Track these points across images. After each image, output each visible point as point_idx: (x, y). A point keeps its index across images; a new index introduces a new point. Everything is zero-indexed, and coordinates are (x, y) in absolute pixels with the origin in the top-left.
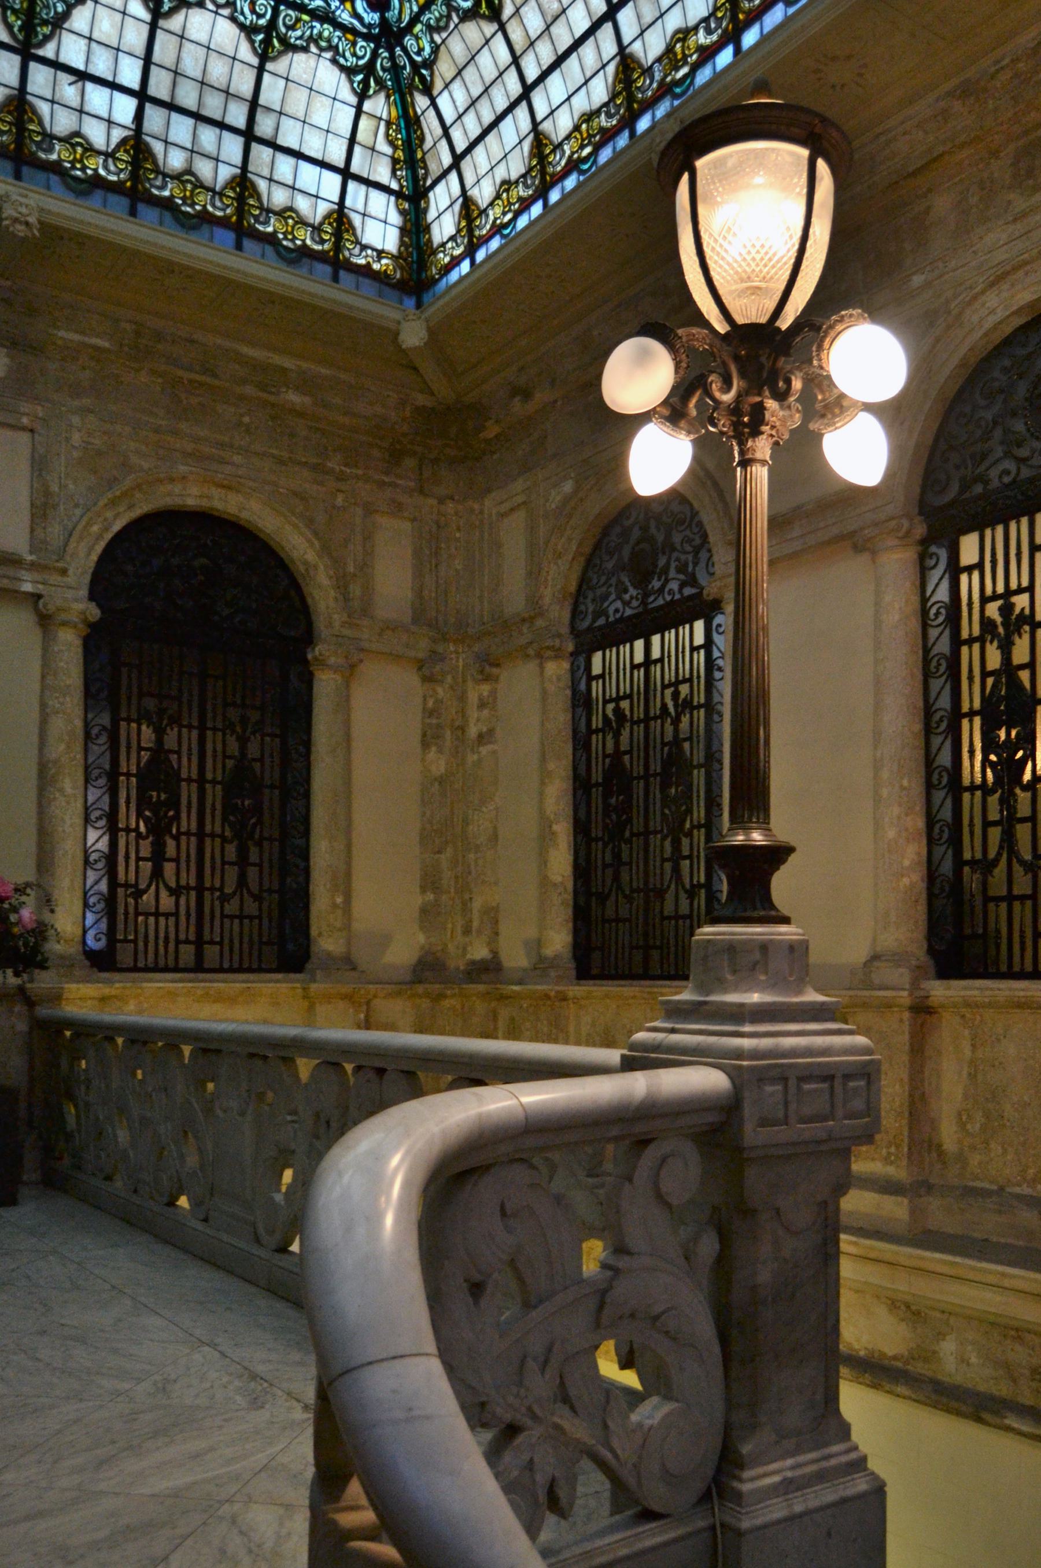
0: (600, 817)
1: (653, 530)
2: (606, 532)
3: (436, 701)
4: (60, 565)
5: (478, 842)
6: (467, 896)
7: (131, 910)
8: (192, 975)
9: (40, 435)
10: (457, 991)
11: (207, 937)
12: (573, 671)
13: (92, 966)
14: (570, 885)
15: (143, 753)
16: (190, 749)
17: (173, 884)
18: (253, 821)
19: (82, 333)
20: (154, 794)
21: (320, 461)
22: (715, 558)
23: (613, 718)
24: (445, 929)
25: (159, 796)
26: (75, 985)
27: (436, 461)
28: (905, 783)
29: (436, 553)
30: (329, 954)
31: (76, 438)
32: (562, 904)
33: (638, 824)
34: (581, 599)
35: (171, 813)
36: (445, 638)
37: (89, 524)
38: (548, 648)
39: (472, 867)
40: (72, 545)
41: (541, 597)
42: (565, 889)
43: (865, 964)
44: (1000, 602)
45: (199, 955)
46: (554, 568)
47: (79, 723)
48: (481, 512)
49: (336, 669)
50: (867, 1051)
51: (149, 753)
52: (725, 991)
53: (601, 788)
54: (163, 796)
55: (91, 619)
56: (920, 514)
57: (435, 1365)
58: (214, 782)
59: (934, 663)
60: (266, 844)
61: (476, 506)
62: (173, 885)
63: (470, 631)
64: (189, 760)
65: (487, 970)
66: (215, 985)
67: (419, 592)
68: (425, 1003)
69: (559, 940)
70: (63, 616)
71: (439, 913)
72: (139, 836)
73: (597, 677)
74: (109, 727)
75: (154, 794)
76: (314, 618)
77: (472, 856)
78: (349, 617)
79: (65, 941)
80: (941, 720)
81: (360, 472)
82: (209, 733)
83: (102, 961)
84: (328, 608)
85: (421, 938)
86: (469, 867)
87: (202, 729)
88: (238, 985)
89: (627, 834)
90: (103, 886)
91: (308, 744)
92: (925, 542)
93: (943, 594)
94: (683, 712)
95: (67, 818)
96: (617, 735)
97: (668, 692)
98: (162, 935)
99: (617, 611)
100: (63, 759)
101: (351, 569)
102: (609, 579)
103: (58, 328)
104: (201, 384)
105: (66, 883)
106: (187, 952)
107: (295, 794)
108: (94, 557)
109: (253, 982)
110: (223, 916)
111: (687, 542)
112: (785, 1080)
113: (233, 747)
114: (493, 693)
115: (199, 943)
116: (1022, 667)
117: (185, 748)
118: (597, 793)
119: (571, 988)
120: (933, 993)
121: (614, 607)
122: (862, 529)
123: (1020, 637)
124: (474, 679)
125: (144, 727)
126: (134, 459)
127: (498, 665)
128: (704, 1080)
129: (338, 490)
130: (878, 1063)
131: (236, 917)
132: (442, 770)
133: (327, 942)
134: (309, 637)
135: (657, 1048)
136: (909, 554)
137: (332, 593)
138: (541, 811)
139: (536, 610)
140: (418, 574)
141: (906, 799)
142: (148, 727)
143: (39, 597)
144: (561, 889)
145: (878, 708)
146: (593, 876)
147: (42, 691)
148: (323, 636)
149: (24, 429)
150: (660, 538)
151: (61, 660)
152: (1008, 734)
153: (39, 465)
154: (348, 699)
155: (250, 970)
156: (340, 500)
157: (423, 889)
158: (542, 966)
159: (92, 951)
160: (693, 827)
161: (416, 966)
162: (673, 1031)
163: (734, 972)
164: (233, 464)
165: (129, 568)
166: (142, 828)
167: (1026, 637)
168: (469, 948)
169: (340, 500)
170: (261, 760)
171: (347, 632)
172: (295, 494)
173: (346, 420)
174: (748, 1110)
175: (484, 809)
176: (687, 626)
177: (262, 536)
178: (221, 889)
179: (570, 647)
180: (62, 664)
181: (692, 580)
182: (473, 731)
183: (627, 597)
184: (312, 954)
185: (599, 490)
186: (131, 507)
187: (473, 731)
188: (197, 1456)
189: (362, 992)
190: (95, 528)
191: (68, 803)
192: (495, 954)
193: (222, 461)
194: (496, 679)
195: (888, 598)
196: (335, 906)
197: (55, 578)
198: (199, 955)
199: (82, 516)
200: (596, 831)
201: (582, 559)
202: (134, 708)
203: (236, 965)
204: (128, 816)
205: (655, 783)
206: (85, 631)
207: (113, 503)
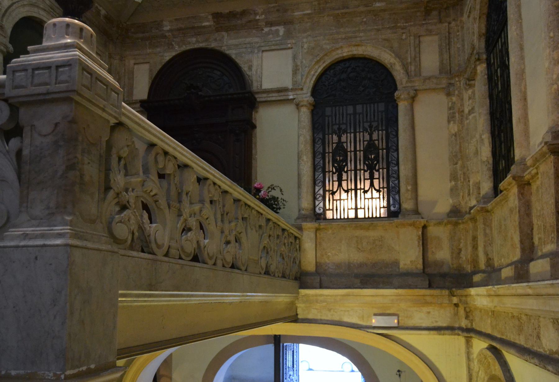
3: (452, 103)
4: (300, 87)
17: (377, 188)
19: (303, 11)
28: (552, 34)
31: (306, 46)
35: (344, 164)
42: (488, 162)
55: (311, 102)
62: (346, 189)
70: (302, 104)
81: (412, 23)
103: (294, 12)
104: (346, 13)
108: (312, 82)
113: (367, 137)
117: (349, 141)
120: (160, 201)
125: (334, 136)
126: (324, 46)
132: (456, 130)
140: (441, 54)
141: (552, 43)
144: (486, 163)
149: (289, 48)
153: (294, 58)
159: (318, 214)
166: (334, 170)
169: (404, 37)
170: (378, 140)
171: (410, 85)
172: (385, 40)
178: (364, 189)
182: (466, 111)
187: (466, 111)
190: (312, 73)
193: (356, 37)
196: (407, 190)
201: (485, 17)
207: (318, 62)
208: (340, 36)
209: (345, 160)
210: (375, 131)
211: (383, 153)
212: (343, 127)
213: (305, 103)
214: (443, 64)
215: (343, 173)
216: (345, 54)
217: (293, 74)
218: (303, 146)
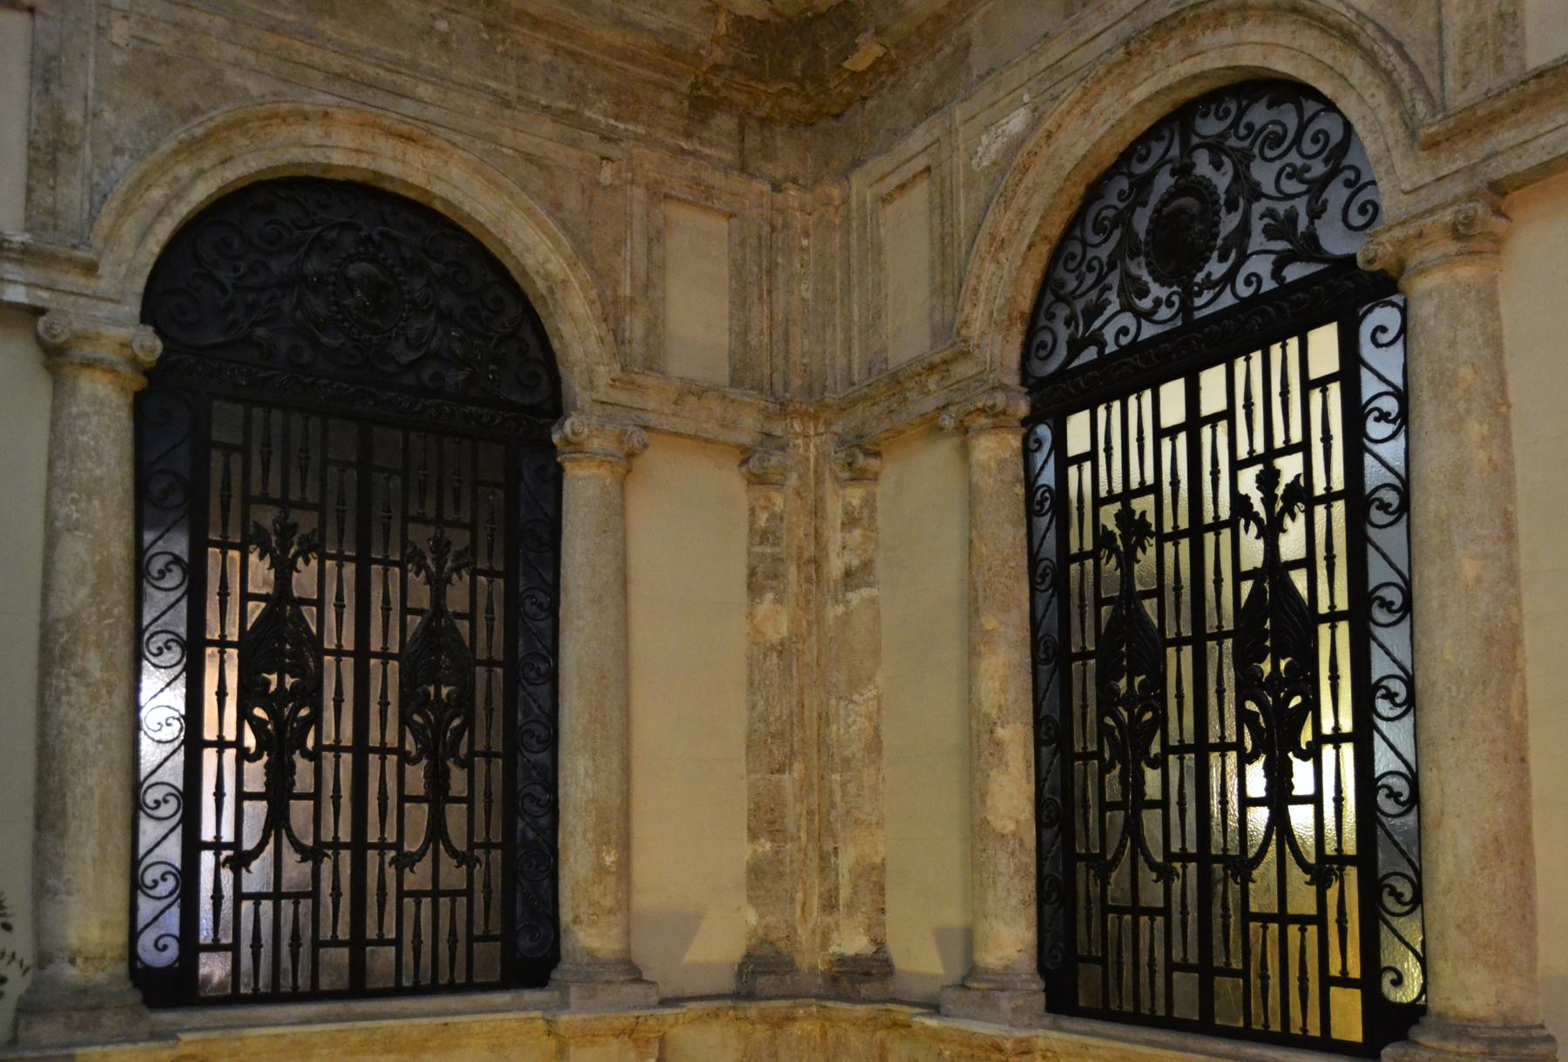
1: (1202, 165)
2: (1094, 191)
3: (773, 517)
5: (848, 753)
6: (829, 845)
8: (336, 1007)
9: (46, 17)
10: (814, 1009)
11: (371, 932)
12: (1027, 452)
15: (251, 604)
16: (340, 597)
17: (461, 845)
18: (456, 722)
20: (274, 678)
21: (572, 107)
23: (1118, 532)
24: (792, 900)
25: (281, 681)
26: (98, 1049)
27: (766, 122)
29: (769, 272)
30: (590, 953)
32: (1017, 871)
33: (1181, 726)
34: (1043, 322)
35: (304, 712)
38: (982, 411)
39: (838, 799)
44: (1117, 506)
45: (358, 965)
46: (990, 267)
48: (845, 201)
49: (604, 459)
51: (263, 605)
53: (1092, 662)
54: (289, 681)
60: (479, 762)
61: (836, 193)
62: (309, 841)
63: (830, 398)
64: (339, 616)
65: (867, 975)
66: (385, 1023)
67: (742, 334)
68: (761, 1033)
69: (1011, 939)
70: (87, 350)
71: (781, 874)
73: (1079, 460)
74: (186, 559)
75: (274, 678)
77: (836, 777)
78: (623, 370)
79: (87, 959)
81: (641, 130)
84: (586, 354)
85: (752, 917)
86: (831, 793)
88: (425, 1021)
89: (1155, 748)
90: (172, 850)
91: (554, 589)
95: (91, 725)
99: (1124, 331)
100: (84, 615)
101: (626, 290)
105: (89, 850)
107: (532, 674)
108: (154, 247)
109: (456, 1013)
110: (401, 894)
111: (1289, 177)
113: (421, 595)
114: (869, 502)
116: (1296, 564)
119: (1041, 1032)
121: (1117, 327)
123: (1293, 517)
124: (836, 479)
125: (253, 558)
126: (233, 77)
127: (877, 455)
129: (603, 158)
131: (425, 894)
132: (784, 631)
133: (587, 933)
134: (555, 407)
137: (595, 330)
139: (953, 343)
140: (740, 303)
142: (261, 557)
143: (38, 311)
144: (1013, 844)
146: (1079, 826)
147: (49, 489)
148: (579, 404)
151: (83, 432)
152: (1275, 665)
153: (45, 73)
154: (622, 511)
157: (753, 835)
158: (973, 981)
159: (148, 969)
161: (742, 965)
165: (225, 275)
167: (1301, 518)
168: (835, 936)
170: (471, 617)
171: (622, 397)
172: (529, 158)
173: (613, 37)
175: (856, 697)
179: (1023, 408)
180: (85, 439)
181: (1309, 248)
182: (835, 567)
183: (1146, 304)
184: (563, 953)
185: (1086, 112)
187: (835, 567)
189: (651, 1022)
190: (157, 194)
191: (94, 698)
192: (880, 944)
194: (875, 478)
196: (601, 870)
197: (73, 280)
198: (358, 965)
200: (1084, 739)
203: (426, 980)
205: (1221, 657)
207: (192, 147)
208: (317, 58)
209: (310, 692)
210: (457, 569)
211: (487, 683)
212: (306, 522)
213: (107, 352)
214: (746, 344)
215: (297, 757)
216: (338, 158)
217: (32, 162)
218: (83, 593)
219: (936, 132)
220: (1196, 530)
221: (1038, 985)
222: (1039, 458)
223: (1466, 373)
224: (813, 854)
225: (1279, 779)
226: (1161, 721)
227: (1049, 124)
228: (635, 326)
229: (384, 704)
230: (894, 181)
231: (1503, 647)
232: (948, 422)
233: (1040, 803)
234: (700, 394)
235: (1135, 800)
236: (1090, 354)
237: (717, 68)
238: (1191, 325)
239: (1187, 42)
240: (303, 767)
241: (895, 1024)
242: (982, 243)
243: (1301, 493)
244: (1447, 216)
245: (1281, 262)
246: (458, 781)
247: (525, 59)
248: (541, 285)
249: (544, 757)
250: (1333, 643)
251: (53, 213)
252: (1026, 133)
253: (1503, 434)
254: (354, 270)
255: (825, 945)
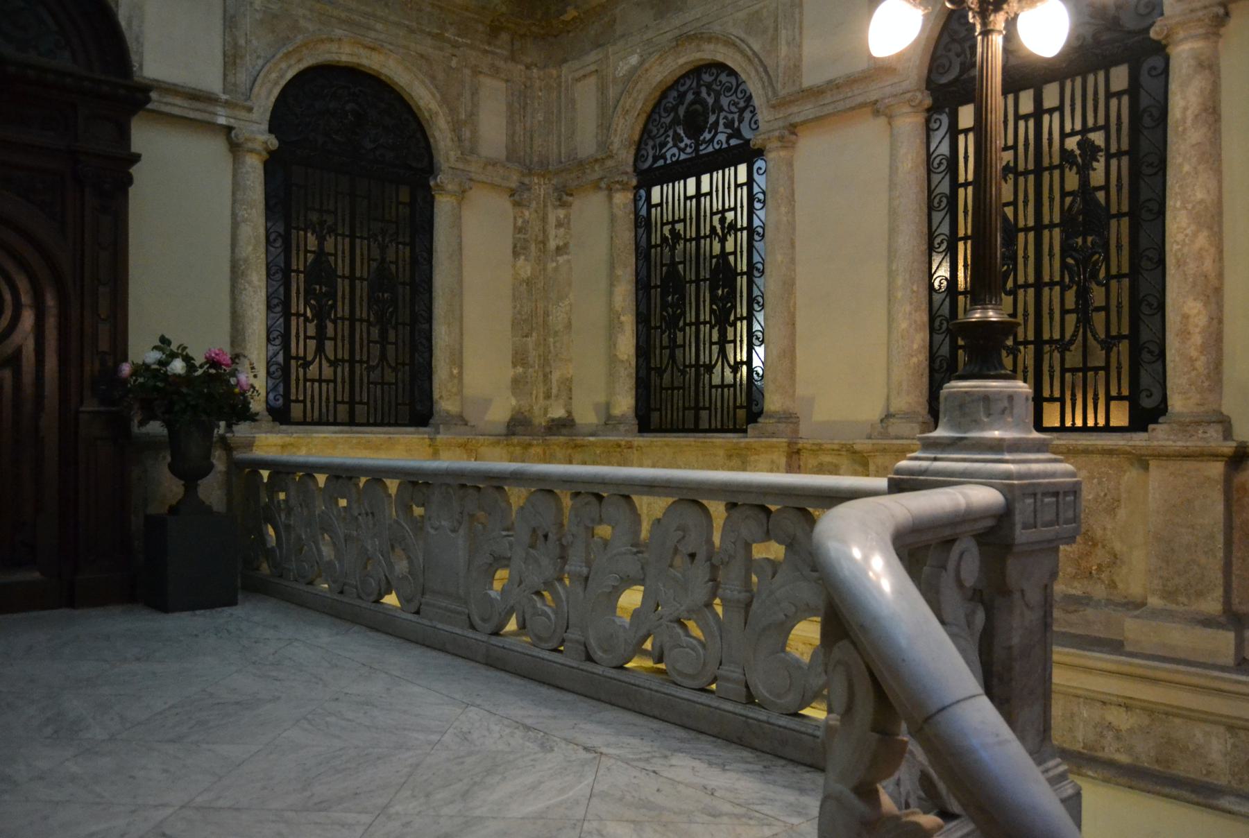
0: (658, 310)
1: (704, 94)
2: (664, 95)
6: (548, 370)
7: (301, 377)
11: (357, 399)
12: (636, 200)
13: (274, 420)
14: (633, 363)
22: (759, 117)
27: (523, 36)
28: (915, 288)
36: (530, 172)
37: (269, 72)
38: (618, 182)
40: (256, 89)
41: (612, 143)
43: (882, 421)
45: (352, 413)
46: (622, 121)
47: (262, 231)
48: (559, 76)
50: (1073, 475)
52: (983, 429)
54: (324, 289)
56: (927, 88)
57: (985, 701)
58: (361, 279)
59: (936, 200)
61: (555, 72)
64: (343, 261)
65: (564, 426)
67: (511, 136)
69: (625, 403)
70: (250, 145)
72: (306, 320)
73: (656, 206)
76: (434, 152)
80: (942, 242)
82: (358, 241)
83: (280, 416)
85: (514, 402)
87: (352, 237)
89: (681, 324)
90: (280, 358)
91: (430, 251)
92: (931, 111)
93: (945, 149)
94: (729, 232)
96: (673, 249)
97: (716, 218)
98: (324, 398)
99: (674, 155)
102: (666, 131)
106: (343, 410)
108: (273, 99)
112: (1035, 495)
113: (376, 253)
114: (567, 216)
115: (352, 403)
116: (731, 253)
118: (656, 294)
121: (671, 153)
122: (883, 99)
123: (1006, 181)
125: (309, 235)
126: (302, 23)
127: (571, 195)
128: (984, 496)
130: (1078, 484)
133: (445, 403)
134: (430, 169)
135: (924, 472)
136: (920, 119)
138: (610, 307)
140: (511, 123)
145: (892, 232)
150: (710, 101)
152: (1085, 241)
155: (389, 425)
156: (454, 63)
157: (514, 365)
158: (610, 422)
160: (736, 319)
162: (935, 459)
163: (989, 415)
164: (375, 30)
166: (309, 314)
167: (1011, 182)
169: (454, 63)
172: (422, 56)
174: (1018, 518)
176: (732, 169)
177: (397, 88)
179: (634, 182)
181: (737, 133)
182: (552, 244)
183: (682, 145)
186: (299, 61)
188: (534, 787)
190: (274, 76)
192: (569, 413)
195: (903, 151)
197: (243, 114)
198: (352, 413)
199: (263, 67)
202: (302, 218)
204: (297, 305)
205: (705, 287)
206: (265, 155)
207: (287, 55)
208: (335, 13)
212: (330, 220)
218: (250, 248)
219: (601, 56)
220: (698, 238)
221: (635, 422)
222: (641, 203)
223: (782, 189)
224: (540, 374)
225: (1083, 294)
226: (684, 313)
227: (647, 65)
228: (466, 133)
229: (362, 300)
230: (582, 73)
231: (789, 285)
232: (603, 185)
233: (638, 347)
234: (494, 165)
235: (673, 345)
236: (661, 162)
237: (503, 14)
238: (698, 157)
239: (698, 45)
240: (330, 326)
241: (576, 446)
242: (619, 109)
243: (733, 227)
244: (777, 133)
245: (729, 137)
246: (392, 336)
247: (420, 10)
248: (426, 114)
249: (426, 326)
250: (742, 282)
251: (235, 85)
252: (636, 65)
253: (792, 211)
254: (348, 107)
255: (545, 414)
